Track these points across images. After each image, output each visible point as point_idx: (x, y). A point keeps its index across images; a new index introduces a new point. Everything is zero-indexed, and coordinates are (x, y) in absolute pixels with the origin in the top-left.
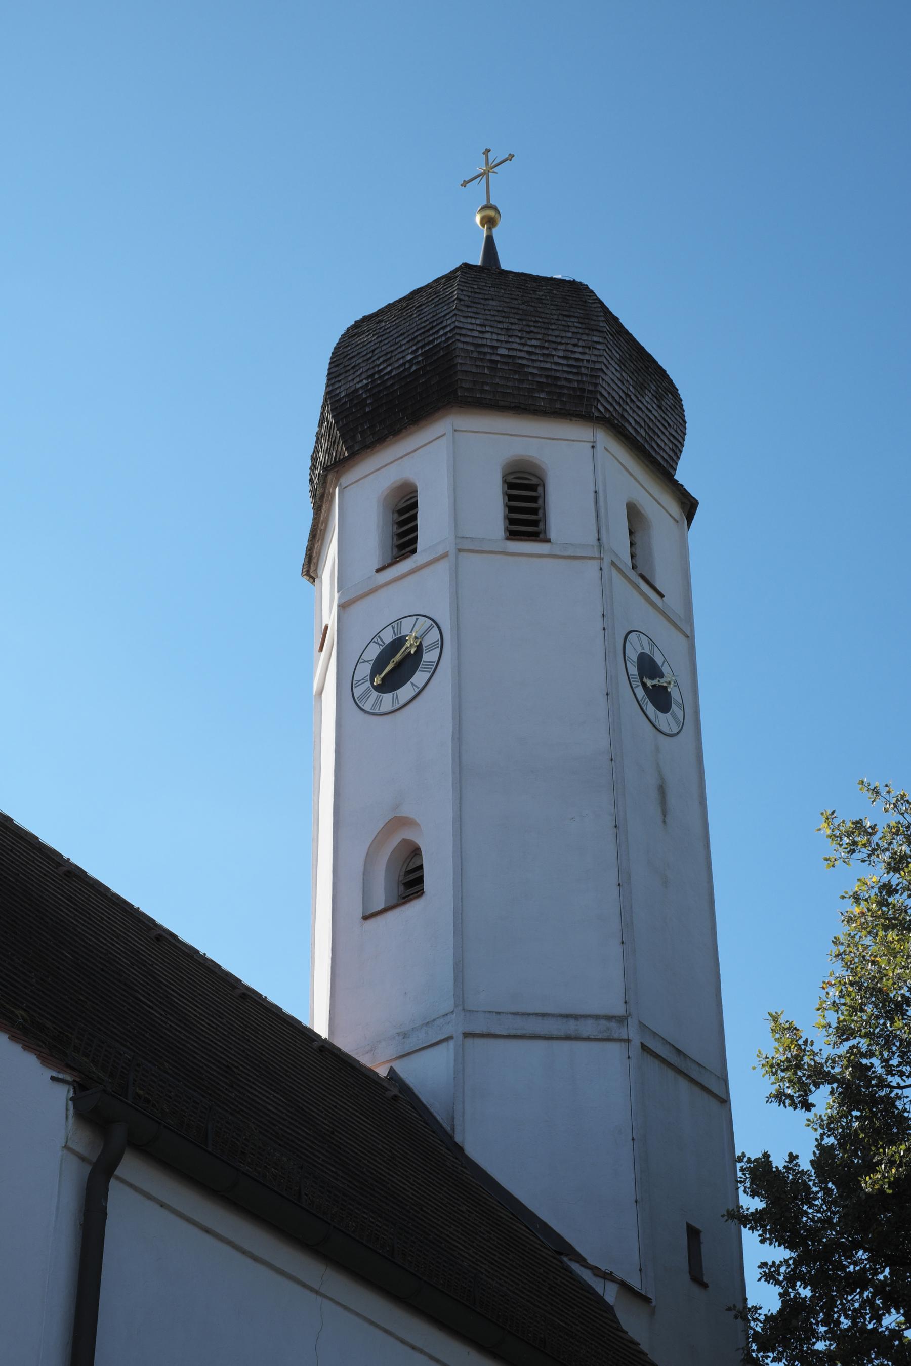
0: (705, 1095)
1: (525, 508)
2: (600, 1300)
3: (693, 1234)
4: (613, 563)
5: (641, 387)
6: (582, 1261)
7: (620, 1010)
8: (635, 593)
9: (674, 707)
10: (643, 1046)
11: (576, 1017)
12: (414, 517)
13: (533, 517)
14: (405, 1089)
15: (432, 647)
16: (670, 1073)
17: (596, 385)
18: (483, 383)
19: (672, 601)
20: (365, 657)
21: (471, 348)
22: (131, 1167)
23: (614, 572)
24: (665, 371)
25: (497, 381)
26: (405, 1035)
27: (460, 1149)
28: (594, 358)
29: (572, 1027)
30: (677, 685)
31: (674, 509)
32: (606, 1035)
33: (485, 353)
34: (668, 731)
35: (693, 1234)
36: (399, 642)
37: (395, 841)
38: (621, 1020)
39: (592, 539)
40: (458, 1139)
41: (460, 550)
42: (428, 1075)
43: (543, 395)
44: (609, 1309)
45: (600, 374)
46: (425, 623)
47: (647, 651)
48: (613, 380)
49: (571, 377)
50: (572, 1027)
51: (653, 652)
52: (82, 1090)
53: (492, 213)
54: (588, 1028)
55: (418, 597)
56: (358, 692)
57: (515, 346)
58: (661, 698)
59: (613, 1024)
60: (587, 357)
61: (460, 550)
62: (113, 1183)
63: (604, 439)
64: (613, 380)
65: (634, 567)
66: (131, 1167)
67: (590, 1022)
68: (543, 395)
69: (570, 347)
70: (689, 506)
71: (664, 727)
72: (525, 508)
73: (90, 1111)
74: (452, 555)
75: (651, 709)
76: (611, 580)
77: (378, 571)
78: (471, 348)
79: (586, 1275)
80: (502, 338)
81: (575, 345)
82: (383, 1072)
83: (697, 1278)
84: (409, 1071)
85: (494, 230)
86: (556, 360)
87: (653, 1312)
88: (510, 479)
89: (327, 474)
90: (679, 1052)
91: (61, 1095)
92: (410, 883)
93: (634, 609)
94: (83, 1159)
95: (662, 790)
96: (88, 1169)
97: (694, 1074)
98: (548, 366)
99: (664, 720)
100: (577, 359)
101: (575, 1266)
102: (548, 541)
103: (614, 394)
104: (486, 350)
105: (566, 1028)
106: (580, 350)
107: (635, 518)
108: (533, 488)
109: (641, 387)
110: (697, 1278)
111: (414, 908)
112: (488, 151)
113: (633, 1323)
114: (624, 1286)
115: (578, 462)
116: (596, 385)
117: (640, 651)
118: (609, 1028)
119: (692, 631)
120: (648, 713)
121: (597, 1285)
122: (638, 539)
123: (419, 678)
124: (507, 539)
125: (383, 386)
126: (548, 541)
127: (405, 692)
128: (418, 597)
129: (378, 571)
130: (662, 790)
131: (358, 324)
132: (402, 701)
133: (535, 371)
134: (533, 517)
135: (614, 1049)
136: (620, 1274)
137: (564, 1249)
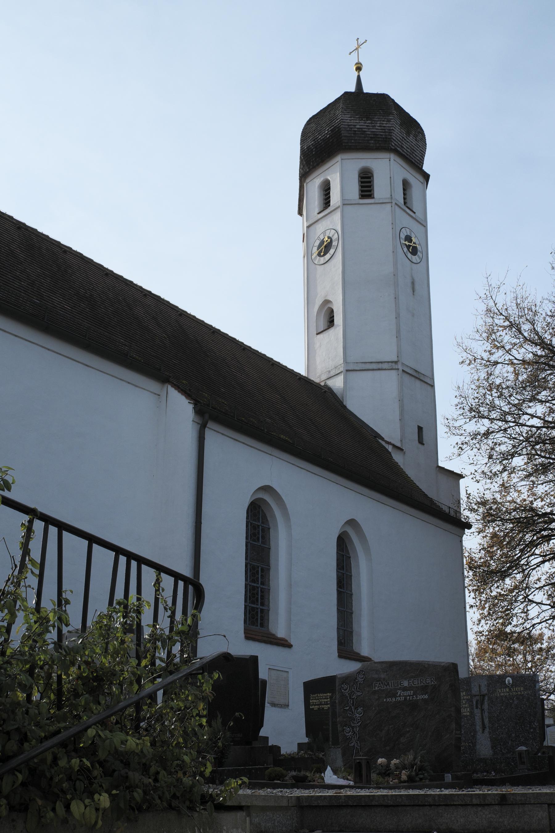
0: (426, 385)
1: (366, 185)
2: (387, 450)
3: (420, 429)
4: (396, 204)
5: (408, 133)
6: (383, 439)
7: (395, 359)
8: (404, 213)
9: (419, 253)
10: (403, 370)
11: (381, 362)
12: (329, 193)
13: (363, 193)
14: (330, 389)
15: (335, 240)
16: (413, 378)
17: (391, 136)
18: (352, 140)
19: (419, 215)
20: (315, 245)
21: (347, 127)
22: (210, 424)
23: (396, 207)
24: (419, 125)
25: (356, 138)
26: (329, 372)
27: (345, 407)
28: (390, 125)
29: (380, 366)
30: (420, 244)
31: (421, 179)
32: (391, 368)
33: (352, 128)
34: (416, 262)
35: (420, 429)
36: (322, 242)
37: (326, 308)
38: (396, 362)
39: (389, 196)
40: (344, 403)
41: (344, 204)
42: (337, 384)
43: (372, 142)
44: (390, 453)
45: (392, 131)
46: (333, 231)
47: (409, 234)
48: (398, 132)
49: (382, 134)
50: (380, 366)
51: (411, 234)
52: (195, 404)
53: (360, 65)
54: (385, 366)
55: (332, 225)
56: (313, 257)
57: (362, 124)
58: (414, 251)
59: (393, 364)
60: (388, 125)
61: (344, 204)
62: (206, 429)
63: (393, 156)
64: (398, 132)
65: (405, 203)
66: (210, 424)
67: (386, 364)
68: (372, 142)
69: (382, 122)
70: (426, 177)
71: (414, 261)
72: (366, 185)
73: (199, 411)
74: (341, 207)
75: (409, 255)
76: (395, 210)
77: (318, 214)
78: (347, 127)
79: (383, 443)
80: (357, 121)
81: (383, 121)
82: (322, 384)
83: (421, 441)
84: (330, 383)
85: (361, 72)
86: (377, 127)
87: (405, 453)
88: (362, 175)
89: (304, 176)
90: (416, 371)
91: (191, 406)
92: (331, 322)
93: (404, 220)
94: (198, 423)
95: (413, 283)
96: (200, 426)
97: (422, 378)
98: (374, 130)
99: (415, 258)
100: (384, 127)
101: (380, 441)
102: (373, 198)
103: (398, 138)
104: (352, 127)
105: (379, 366)
106: (385, 122)
107: (406, 185)
108: (369, 178)
109: (408, 133)
110: (421, 441)
111: (331, 331)
112: (358, 39)
113: (397, 457)
114: (394, 446)
115: (386, 169)
116: (391, 136)
117: (406, 234)
118: (393, 365)
119: (427, 224)
120: (408, 256)
121: (386, 446)
122: (408, 192)
123: (332, 251)
124: (360, 198)
125: (323, 141)
126: (373, 198)
127: (328, 256)
128: (332, 225)
129: (318, 214)
130: (413, 283)
131: (311, 119)
132: (327, 260)
133: (369, 133)
134: (363, 193)
135: (394, 372)
136: (393, 442)
137: (377, 436)
